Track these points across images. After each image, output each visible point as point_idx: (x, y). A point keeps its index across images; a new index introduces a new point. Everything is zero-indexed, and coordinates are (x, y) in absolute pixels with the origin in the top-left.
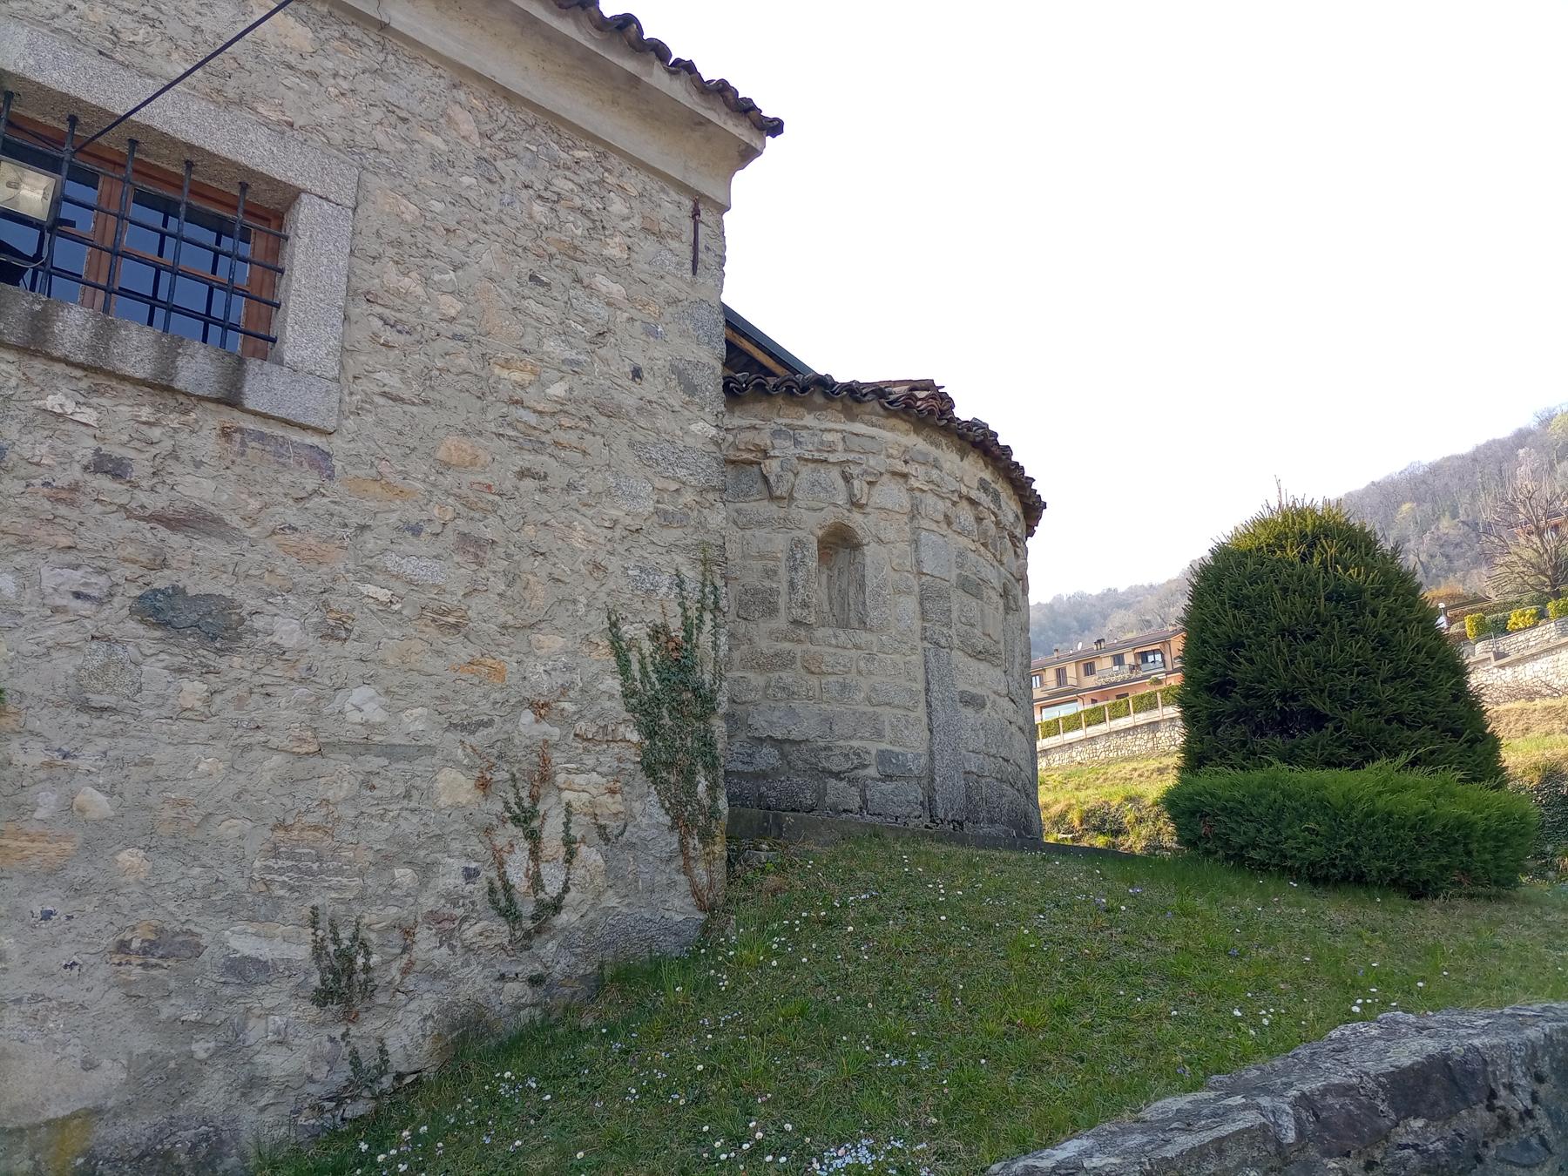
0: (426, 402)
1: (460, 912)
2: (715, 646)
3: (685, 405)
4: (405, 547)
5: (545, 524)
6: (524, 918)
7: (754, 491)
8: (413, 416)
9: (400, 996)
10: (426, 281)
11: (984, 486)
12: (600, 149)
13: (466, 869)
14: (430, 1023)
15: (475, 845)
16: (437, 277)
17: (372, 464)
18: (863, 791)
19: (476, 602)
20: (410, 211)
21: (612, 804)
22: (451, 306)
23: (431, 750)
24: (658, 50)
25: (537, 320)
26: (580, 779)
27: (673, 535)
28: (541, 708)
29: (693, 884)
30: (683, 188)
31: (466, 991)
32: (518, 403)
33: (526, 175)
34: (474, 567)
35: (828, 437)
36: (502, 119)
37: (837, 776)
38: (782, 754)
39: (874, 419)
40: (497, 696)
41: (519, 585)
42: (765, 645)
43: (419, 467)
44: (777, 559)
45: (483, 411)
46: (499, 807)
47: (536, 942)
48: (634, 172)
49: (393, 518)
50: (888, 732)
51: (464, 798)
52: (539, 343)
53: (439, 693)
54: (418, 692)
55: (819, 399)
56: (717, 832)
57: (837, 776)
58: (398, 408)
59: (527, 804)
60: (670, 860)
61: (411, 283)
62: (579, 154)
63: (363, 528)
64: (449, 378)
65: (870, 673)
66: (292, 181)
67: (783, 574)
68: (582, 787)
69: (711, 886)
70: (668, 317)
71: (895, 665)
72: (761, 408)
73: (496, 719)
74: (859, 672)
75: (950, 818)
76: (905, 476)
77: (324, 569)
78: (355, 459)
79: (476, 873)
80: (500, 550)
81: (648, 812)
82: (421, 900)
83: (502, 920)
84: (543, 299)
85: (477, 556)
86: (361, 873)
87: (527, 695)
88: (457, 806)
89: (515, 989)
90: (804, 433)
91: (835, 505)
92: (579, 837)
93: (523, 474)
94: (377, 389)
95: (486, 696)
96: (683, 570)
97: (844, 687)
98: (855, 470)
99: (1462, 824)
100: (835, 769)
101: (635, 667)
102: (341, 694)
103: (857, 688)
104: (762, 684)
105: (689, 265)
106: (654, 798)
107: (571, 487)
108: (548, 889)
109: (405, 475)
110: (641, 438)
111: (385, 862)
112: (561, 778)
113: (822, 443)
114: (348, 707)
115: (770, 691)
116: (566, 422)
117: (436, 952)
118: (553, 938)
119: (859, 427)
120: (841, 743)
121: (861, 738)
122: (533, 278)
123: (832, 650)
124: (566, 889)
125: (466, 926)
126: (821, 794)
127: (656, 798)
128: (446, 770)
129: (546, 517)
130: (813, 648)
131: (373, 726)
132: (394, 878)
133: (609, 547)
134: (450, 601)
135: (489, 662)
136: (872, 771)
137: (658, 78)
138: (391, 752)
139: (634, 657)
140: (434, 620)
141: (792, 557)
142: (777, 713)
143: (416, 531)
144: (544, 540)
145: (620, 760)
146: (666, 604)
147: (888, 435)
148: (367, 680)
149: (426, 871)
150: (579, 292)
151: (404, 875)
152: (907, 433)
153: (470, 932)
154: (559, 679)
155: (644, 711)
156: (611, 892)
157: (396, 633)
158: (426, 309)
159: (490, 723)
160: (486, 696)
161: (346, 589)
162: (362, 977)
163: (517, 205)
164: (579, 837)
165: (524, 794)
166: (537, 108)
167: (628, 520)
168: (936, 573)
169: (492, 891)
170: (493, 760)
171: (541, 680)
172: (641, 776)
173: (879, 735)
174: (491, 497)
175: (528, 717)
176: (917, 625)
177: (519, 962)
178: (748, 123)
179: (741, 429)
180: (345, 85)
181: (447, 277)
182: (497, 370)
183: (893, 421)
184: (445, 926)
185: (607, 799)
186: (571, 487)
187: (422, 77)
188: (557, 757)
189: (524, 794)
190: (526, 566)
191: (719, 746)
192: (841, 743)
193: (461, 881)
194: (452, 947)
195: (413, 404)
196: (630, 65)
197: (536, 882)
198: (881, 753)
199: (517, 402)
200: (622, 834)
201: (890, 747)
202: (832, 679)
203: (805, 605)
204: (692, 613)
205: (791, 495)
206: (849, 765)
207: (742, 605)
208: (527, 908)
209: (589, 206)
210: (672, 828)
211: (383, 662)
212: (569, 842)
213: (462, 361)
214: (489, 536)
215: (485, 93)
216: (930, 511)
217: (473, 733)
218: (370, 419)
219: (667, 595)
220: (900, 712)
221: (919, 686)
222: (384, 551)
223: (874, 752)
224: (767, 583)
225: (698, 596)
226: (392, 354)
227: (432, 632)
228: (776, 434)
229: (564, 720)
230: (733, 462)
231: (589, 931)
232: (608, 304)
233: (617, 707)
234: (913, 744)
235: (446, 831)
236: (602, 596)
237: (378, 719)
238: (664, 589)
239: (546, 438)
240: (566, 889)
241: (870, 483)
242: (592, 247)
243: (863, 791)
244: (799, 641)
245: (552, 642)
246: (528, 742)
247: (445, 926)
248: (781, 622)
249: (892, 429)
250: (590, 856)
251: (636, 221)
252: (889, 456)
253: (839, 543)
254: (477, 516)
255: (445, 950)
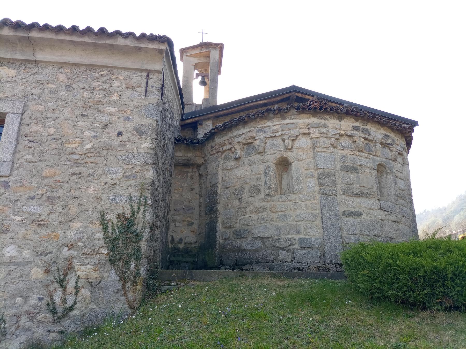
0: (40, 161)
1: (36, 311)
2: (144, 217)
3: (139, 139)
4: (30, 204)
5: (79, 188)
6: (59, 313)
7: (253, 152)
8: (36, 166)
9: (14, 336)
10: (44, 126)
11: (356, 128)
12: (110, 69)
13: (39, 298)
14: (22, 345)
15: (43, 290)
16: (48, 124)
17: (21, 182)
18: (293, 254)
19: (52, 216)
20: (41, 108)
21: (95, 275)
22: (51, 131)
23: (30, 262)
24: (117, 33)
25: (82, 127)
26: (83, 267)
27: (129, 183)
28: (71, 246)
29: (127, 300)
30: (142, 70)
31: (36, 335)
32: (72, 153)
33: (82, 85)
34: (52, 206)
35: (275, 128)
36: (75, 72)
37: (283, 249)
38: (263, 242)
39: (293, 117)
40: (55, 244)
41: (67, 209)
42: (257, 204)
43: (36, 180)
44: (261, 174)
45: (60, 158)
46: (52, 278)
47: (62, 321)
48: (123, 72)
49: (26, 196)
50: (303, 230)
51: (39, 276)
52: (82, 133)
53: (35, 245)
54: (28, 246)
55: (271, 115)
56: (138, 281)
57: (283, 249)
58: (31, 164)
59: (62, 277)
60: (117, 292)
61: (40, 128)
62: (102, 73)
63: (17, 201)
64: (49, 152)
65: (295, 209)
66: (5, 112)
67: (263, 179)
68: (84, 270)
69: (135, 300)
70: (134, 112)
71: (306, 205)
72: (252, 124)
73: (54, 251)
74: (291, 210)
75: (334, 262)
76: (309, 134)
77: (4, 214)
78: (15, 182)
79: (43, 299)
80: (61, 199)
81: (111, 276)
82: (24, 307)
83: (50, 313)
84: (85, 120)
85: (52, 202)
86: (5, 300)
87: (66, 242)
88: (37, 279)
89: (53, 335)
90: (267, 128)
91: (280, 151)
92: (81, 286)
93: (72, 174)
94: (24, 161)
95: (51, 244)
96: (133, 193)
97: (285, 216)
98: (286, 137)
99: (436, 271)
100: (282, 246)
101: (110, 229)
102: (4, 249)
103: (290, 216)
104: (257, 218)
105: (144, 94)
106: (113, 271)
107: (90, 175)
108: (68, 303)
109: (31, 183)
110: (120, 154)
111: (13, 296)
112: (76, 267)
113: (273, 130)
114: (5, 252)
115: (259, 221)
116: (89, 155)
117: (28, 323)
118: (69, 319)
119: (287, 121)
120: (284, 237)
121: (292, 234)
122: (82, 115)
123: (280, 203)
124: (75, 303)
125: (38, 315)
126: (277, 256)
127: (114, 271)
128: (34, 268)
129: (79, 186)
130: (273, 203)
131: (12, 257)
132: (15, 301)
133: (103, 191)
134: (42, 217)
135: (54, 234)
136: (297, 246)
137: (121, 41)
138: (18, 264)
139: (110, 225)
140: (36, 224)
141: (265, 172)
142: (261, 228)
143: (33, 198)
144: (77, 193)
145: (99, 260)
146: (124, 206)
147: (300, 121)
148: (12, 244)
149: (26, 299)
150: (100, 114)
151: (19, 300)
152: (309, 118)
153: (39, 317)
154: (79, 236)
155: (112, 243)
156: (92, 304)
157: (23, 229)
158: (43, 134)
159: (51, 253)
160: (51, 244)
161: (9, 219)
162: (3, 330)
163: (78, 95)
164: (81, 286)
165: (61, 274)
166: (85, 65)
167: (112, 181)
168: (326, 167)
169: (48, 304)
170: (51, 264)
171: (72, 236)
172: (108, 264)
173: (299, 232)
174: (59, 184)
175: (66, 249)
176: (317, 188)
177: (56, 327)
178: (157, 42)
179: (247, 132)
180: (24, 80)
181: (51, 123)
182: (66, 145)
183: (301, 115)
184: (31, 316)
185: (93, 273)
186: (90, 175)
187: (50, 70)
188: (75, 261)
189: (61, 274)
190: (70, 202)
191: (143, 251)
192: (284, 237)
193: (37, 301)
194: (33, 322)
195: (36, 162)
196: (108, 42)
197: (64, 301)
198: (300, 239)
199: (72, 153)
200: (98, 284)
201: (304, 237)
202: (280, 213)
203: (270, 188)
204: (136, 208)
205: (264, 150)
206: (287, 245)
207: (250, 192)
208: (60, 310)
209: (105, 87)
210: (119, 281)
211: (18, 238)
212: (77, 289)
213: (54, 146)
214: (58, 196)
215: (70, 67)
216: (322, 144)
217: (46, 256)
218: (21, 169)
219: (125, 203)
220: (308, 223)
221: (318, 212)
222: (23, 206)
223: (297, 239)
224: (258, 183)
225: (138, 201)
226: (31, 150)
227: (35, 227)
228: (258, 131)
229: (79, 249)
230: (246, 144)
231: (83, 316)
232: (110, 115)
233: (102, 243)
234: (315, 233)
235: (33, 286)
236: (99, 207)
237: (14, 255)
238: (124, 201)
239: (82, 162)
240: (75, 303)
241: (293, 140)
242: (107, 99)
243: (293, 254)
244: (268, 201)
245: (77, 225)
246: (65, 257)
247: (31, 316)
248: (262, 196)
249: (302, 118)
250: (85, 292)
251: (123, 87)
252: (301, 128)
253: (284, 164)
254: (55, 190)
255: (30, 322)
